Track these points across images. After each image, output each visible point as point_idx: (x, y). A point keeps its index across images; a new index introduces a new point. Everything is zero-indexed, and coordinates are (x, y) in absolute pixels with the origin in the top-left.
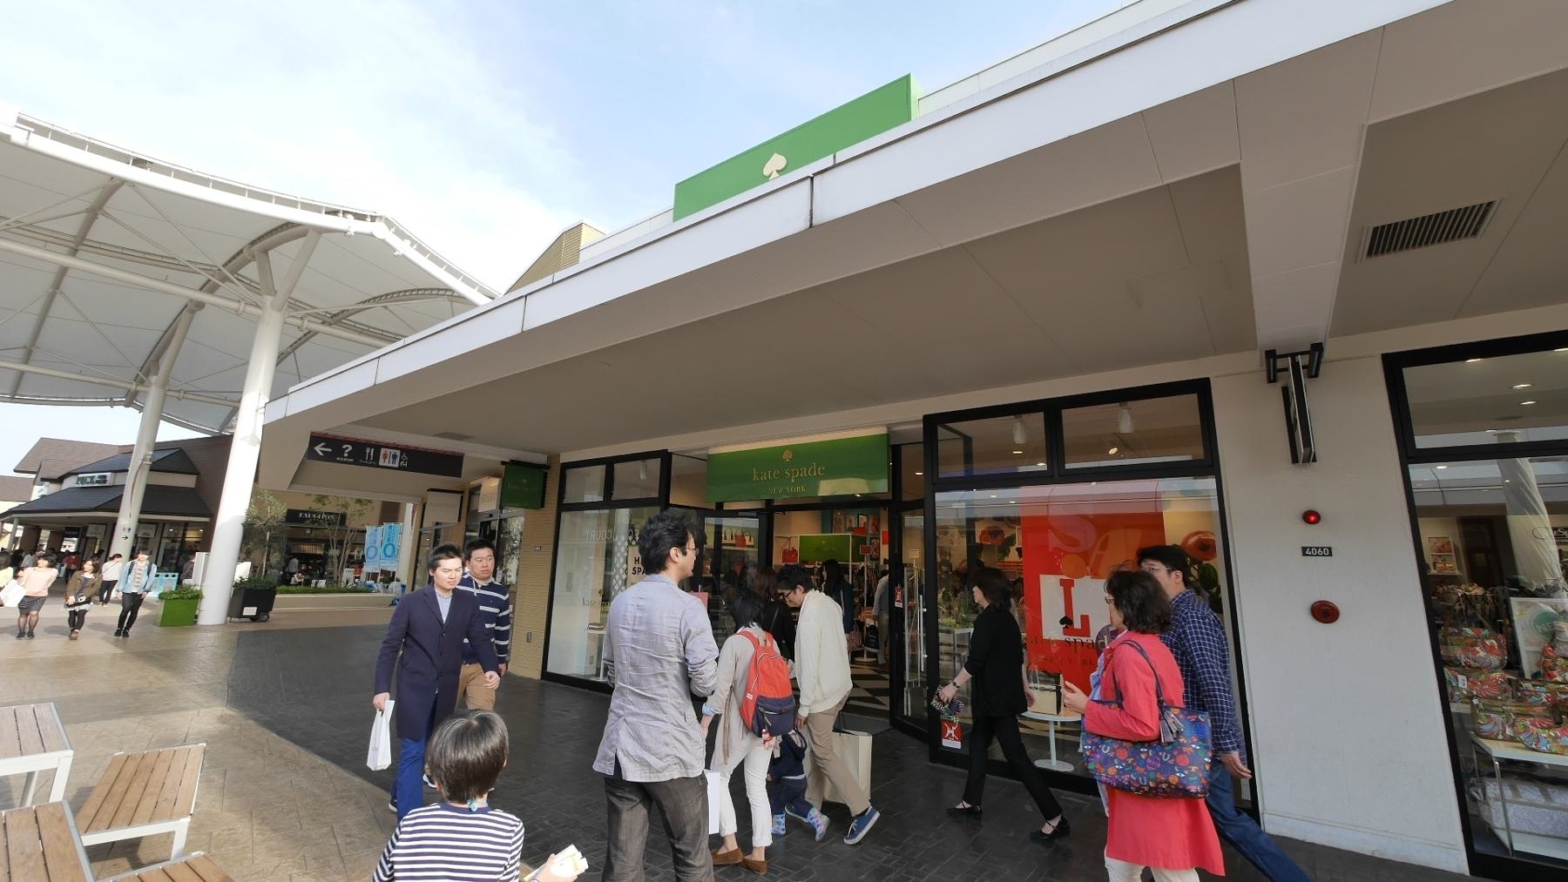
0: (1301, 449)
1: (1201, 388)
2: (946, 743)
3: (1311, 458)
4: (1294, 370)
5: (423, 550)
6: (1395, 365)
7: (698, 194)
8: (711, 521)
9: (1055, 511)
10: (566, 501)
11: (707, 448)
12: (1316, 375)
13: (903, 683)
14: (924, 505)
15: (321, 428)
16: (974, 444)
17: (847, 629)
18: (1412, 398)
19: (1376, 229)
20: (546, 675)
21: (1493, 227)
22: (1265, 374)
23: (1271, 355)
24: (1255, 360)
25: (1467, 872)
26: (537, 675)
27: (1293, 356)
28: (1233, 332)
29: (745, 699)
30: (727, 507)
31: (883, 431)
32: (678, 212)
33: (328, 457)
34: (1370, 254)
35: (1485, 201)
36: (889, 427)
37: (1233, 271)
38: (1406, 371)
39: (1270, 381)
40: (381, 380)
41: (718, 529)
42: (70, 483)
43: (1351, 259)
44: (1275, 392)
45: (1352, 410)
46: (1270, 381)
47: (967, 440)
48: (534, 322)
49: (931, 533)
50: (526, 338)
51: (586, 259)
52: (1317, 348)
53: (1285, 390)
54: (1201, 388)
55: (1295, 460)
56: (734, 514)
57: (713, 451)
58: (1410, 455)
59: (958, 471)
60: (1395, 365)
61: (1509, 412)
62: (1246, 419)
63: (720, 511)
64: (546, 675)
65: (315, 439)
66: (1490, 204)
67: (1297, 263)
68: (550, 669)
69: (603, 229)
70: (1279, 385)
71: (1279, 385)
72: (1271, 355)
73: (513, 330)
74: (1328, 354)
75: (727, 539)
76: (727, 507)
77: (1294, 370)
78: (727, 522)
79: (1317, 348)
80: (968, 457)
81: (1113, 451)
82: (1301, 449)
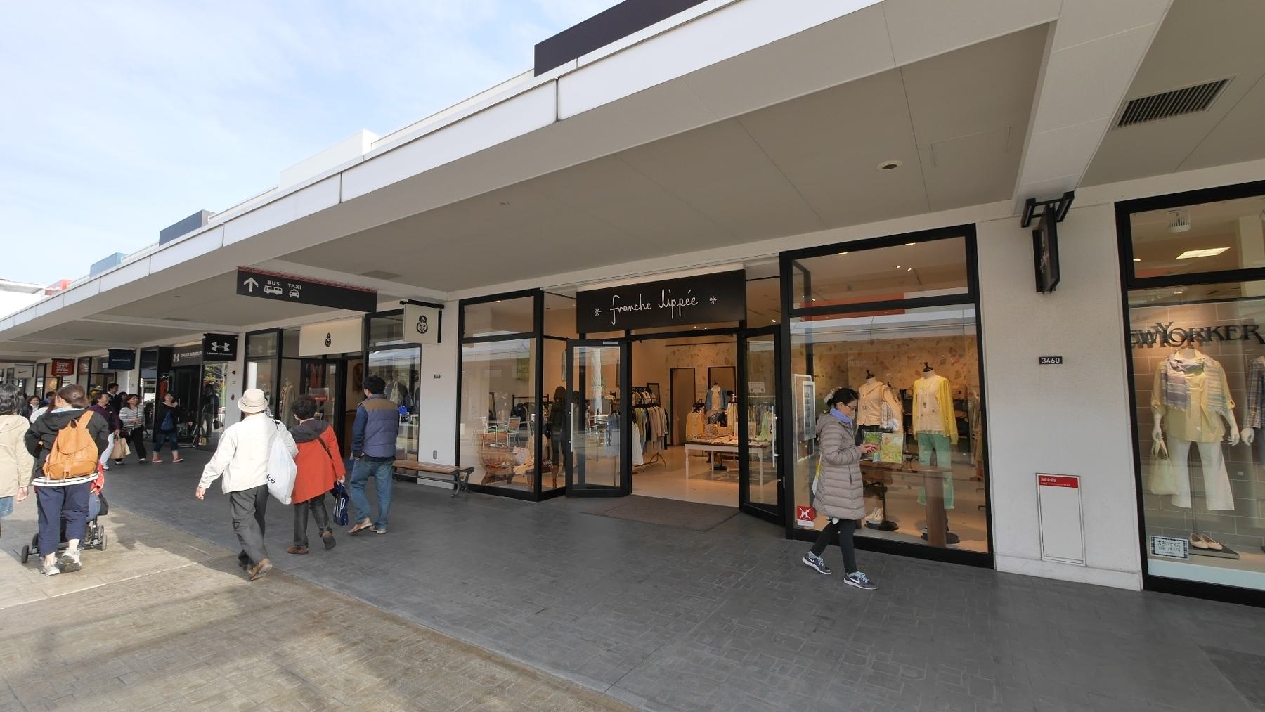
0: (1046, 279)
1: (968, 232)
2: (800, 523)
3: (1052, 288)
4: (1045, 218)
5: (286, 389)
6: (1124, 210)
7: (168, 235)
8: (577, 350)
10: (466, 336)
15: (249, 263)
16: (813, 278)
17: (11, 413)
18: (546, 309)
20: (1152, 583)
21: (1220, 102)
23: (1031, 203)
24: (1009, 209)
25: (288, 501)
26: (1136, 583)
27: (1047, 203)
31: (739, 267)
32: (161, 243)
33: (259, 292)
36: (744, 263)
40: (154, 271)
43: (1111, 129)
44: (1027, 235)
45: (1090, 243)
46: (1024, 226)
47: (807, 274)
48: (105, 288)
50: (152, 278)
51: (124, 263)
53: (1037, 235)
54: (968, 232)
58: (1130, 281)
60: (1124, 210)
61: (919, 279)
62: (1004, 259)
63: (583, 342)
64: (1152, 583)
65: (243, 274)
66: (1223, 82)
67: (1066, 137)
69: (216, 204)
70: (1029, 230)
71: (1029, 230)
72: (1031, 203)
79: (1070, 196)
80: (808, 290)
82: (1046, 279)
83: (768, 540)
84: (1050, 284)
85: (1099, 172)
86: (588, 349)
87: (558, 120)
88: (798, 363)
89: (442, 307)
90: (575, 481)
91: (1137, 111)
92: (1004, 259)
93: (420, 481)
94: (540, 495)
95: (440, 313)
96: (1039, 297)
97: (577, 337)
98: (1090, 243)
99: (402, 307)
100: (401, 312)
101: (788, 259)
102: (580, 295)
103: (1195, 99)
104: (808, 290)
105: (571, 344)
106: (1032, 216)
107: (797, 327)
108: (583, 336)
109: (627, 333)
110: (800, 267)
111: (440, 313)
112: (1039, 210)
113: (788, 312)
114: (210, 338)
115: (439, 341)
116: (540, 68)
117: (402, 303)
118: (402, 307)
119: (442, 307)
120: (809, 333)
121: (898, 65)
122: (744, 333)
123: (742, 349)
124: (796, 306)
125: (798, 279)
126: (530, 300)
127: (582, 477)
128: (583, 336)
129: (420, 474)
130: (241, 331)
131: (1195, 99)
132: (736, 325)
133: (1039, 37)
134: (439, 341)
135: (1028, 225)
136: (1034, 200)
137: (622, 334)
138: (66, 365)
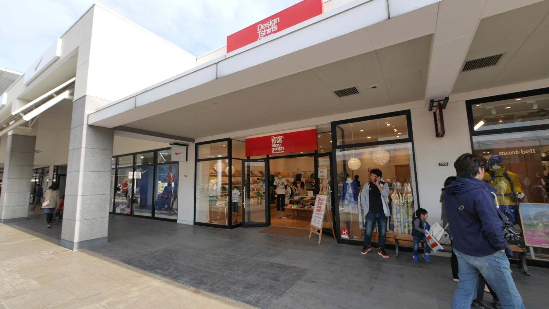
0: (440, 133)
1: (407, 113)
2: (343, 236)
3: (442, 136)
4: (439, 106)
6: (470, 104)
13: (378, 226)
16: (345, 132)
19: (55, 166)
20: (195, 223)
21: (501, 63)
22: (427, 109)
23: (432, 101)
26: (192, 223)
27: (438, 101)
29: (53, 182)
30: (251, 158)
31: (314, 128)
35: (500, 53)
37: (422, 75)
38: (473, 106)
41: (249, 167)
42: (55, 176)
43: (460, 73)
44: (431, 113)
45: (456, 116)
47: (342, 130)
53: (435, 114)
54: (407, 113)
55: (438, 135)
56: (256, 160)
58: (473, 133)
60: (470, 104)
62: (422, 122)
63: (249, 160)
66: (501, 55)
67: (443, 73)
68: (197, 221)
70: (432, 112)
71: (432, 112)
72: (432, 101)
73: (132, 106)
75: (251, 169)
76: (251, 158)
77: (439, 106)
78: (251, 164)
79: (447, 99)
81: (501, 121)
82: (440, 133)
84: (441, 134)
85: (458, 88)
87: (389, 18)
90: (246, 220)
91: (469, 66)
92: (422, 122)
94: (231, 226)
95: (187, 148)
97: (246, 158)
98: (456, 116)
99: (171, 146)
100: (170, 148)
101: (334, 125)
102: (246, 140)
103: (354, 91)
104: (343, 137)
105: (243, 161)
106: (433, 106)
107: (339, 153)
108: (248, 158)
109: (268, 156)
110: (339, 128)
111: (187, 148)
113: (335, 146)
115: (187, 160)
116: (230, 48)
117: (171, 144)
118: (171, 146)
119: (49, 167)
120: (344, 156)
121: (374, 49)
122: (316, 156)
124: (338, 144)
125: (339, 133)
127: (249, 218)
128: (248, 158)
132: (314, 152)
133: (429, 38)
134: (187, 160)
137: (265, 157)
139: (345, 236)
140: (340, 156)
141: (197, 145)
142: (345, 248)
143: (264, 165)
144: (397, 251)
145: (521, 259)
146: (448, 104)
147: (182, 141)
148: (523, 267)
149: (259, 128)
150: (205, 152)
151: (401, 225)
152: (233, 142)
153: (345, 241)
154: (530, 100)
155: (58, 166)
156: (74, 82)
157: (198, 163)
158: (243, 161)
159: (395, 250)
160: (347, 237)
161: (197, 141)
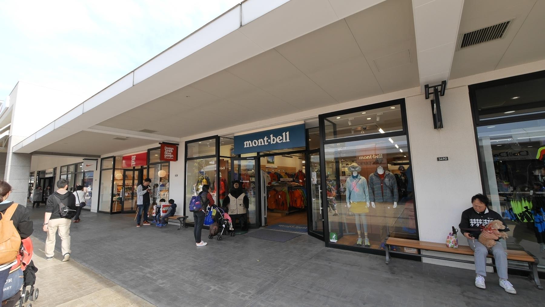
0: (438, 122)
1: (401, 102)
2: (331, 240)
3: (441, 126)
4: (436, 93)
8: (236, 162)
9: (506, 143)
11: (233, 134)
12: (443, 95)
14: (319, 151)
21: (509, 33)
22: (424, 95)
23: (427, 87)
24: (419, 90)
26: (96, 211)
27: (435, 87)
28: (411, 80)
30: (243, 156)
31: (302, 122)
34: (462, 47)
39: (426, 98)
40: (85, 111)
43: (456, 50)
46: (426, 98)
47: (334, 125)
49: (323, 162)
52: (444, 83)
53: (432, 102)
54: (401, 102)
55: (436, 127)
56: (245, 159)
57: (236, 135)
59: (332, 138)
62: (418, 114)
66: (508, 22)
67: (436, 55)
68: (100, 210)
70: (429, 101)
72: (427, 87)
74: (448, 86)
76: (243, 156)
77: (436, 93)
79: (444, 83)
82: (438, 122)
83: (320, 245)
86: (112, 170)
88: (270, 159)
89: (178, 145)
91: (468, 40)
92: (418, 114)
93: (425, 260)
96: (442, 131)
101: (322, 118)
102: (235, 137)
103: (496, 31)
109: (258, 153)
111: (177, 148)
112: (431, 90)
114: (164, 145)
119: (178, 145)
123: (308, 159)
125: (328, 129)
126: (112, 159)
129: (423, 253)
130: (181, 142)
131: (496, 31)
135: (428, 98)
136: (428, 85)
137: (255, 154)
138: (171, 150)
139: (333, 240)
140: (330, 154)
141: (102, 159)
142: (336, 253)
143: (254, 163)
144: (387, 257)
145: (532, 269)
146: (446, 91)
147: (88, 157)
148: (534, 279)
149: (258, 122)
150: (194, 151)
151: (160, 207)
152: (116, 158)
153: (334, 246)
154: (379, 112)
155: (39, 172)
156: (10, 126)
157: (103, 172)
158: (125, 170)
159: (385, 255)
160: (335, 241)
161: (102, 157)
